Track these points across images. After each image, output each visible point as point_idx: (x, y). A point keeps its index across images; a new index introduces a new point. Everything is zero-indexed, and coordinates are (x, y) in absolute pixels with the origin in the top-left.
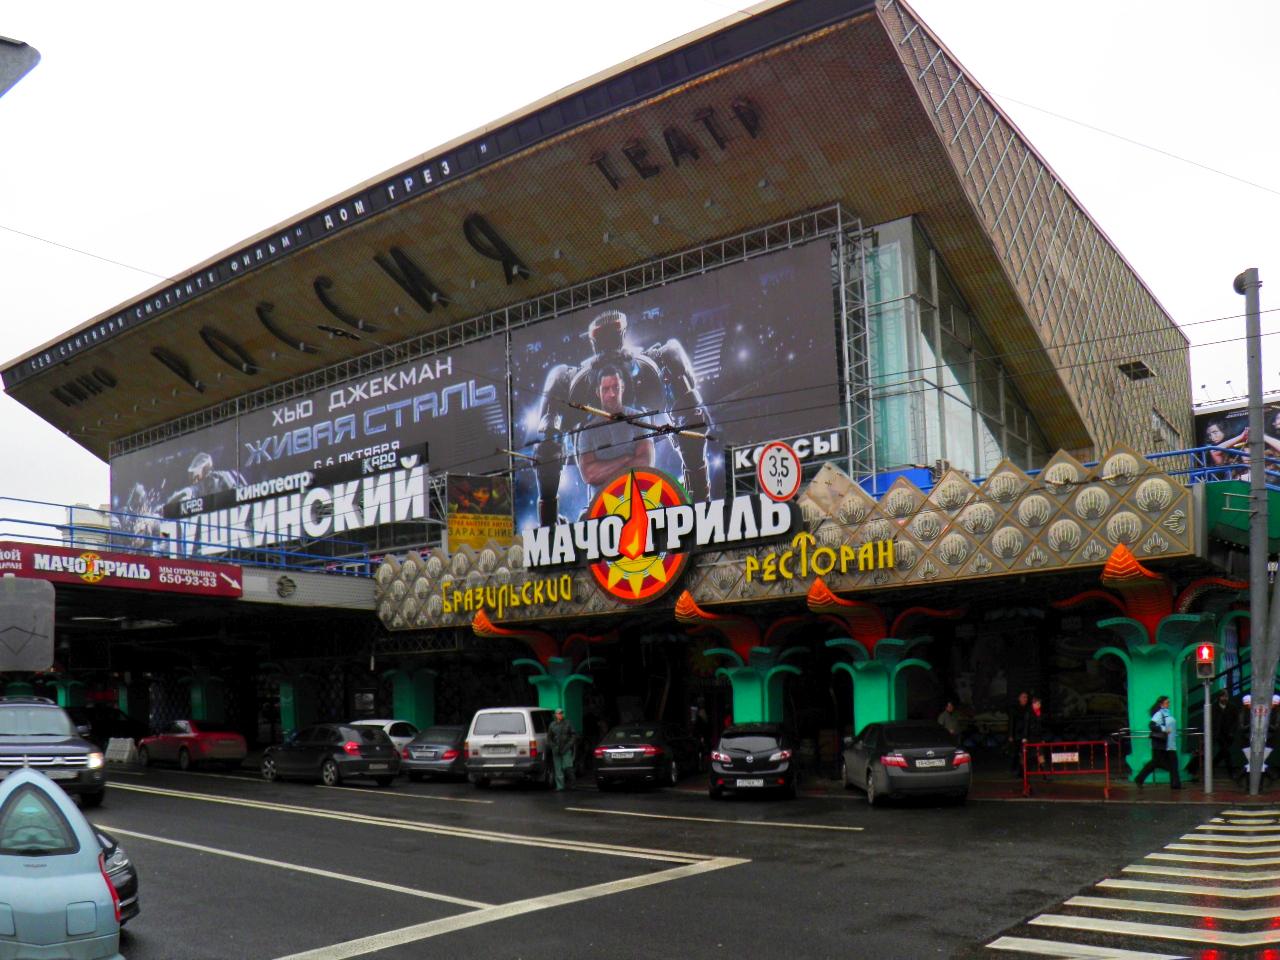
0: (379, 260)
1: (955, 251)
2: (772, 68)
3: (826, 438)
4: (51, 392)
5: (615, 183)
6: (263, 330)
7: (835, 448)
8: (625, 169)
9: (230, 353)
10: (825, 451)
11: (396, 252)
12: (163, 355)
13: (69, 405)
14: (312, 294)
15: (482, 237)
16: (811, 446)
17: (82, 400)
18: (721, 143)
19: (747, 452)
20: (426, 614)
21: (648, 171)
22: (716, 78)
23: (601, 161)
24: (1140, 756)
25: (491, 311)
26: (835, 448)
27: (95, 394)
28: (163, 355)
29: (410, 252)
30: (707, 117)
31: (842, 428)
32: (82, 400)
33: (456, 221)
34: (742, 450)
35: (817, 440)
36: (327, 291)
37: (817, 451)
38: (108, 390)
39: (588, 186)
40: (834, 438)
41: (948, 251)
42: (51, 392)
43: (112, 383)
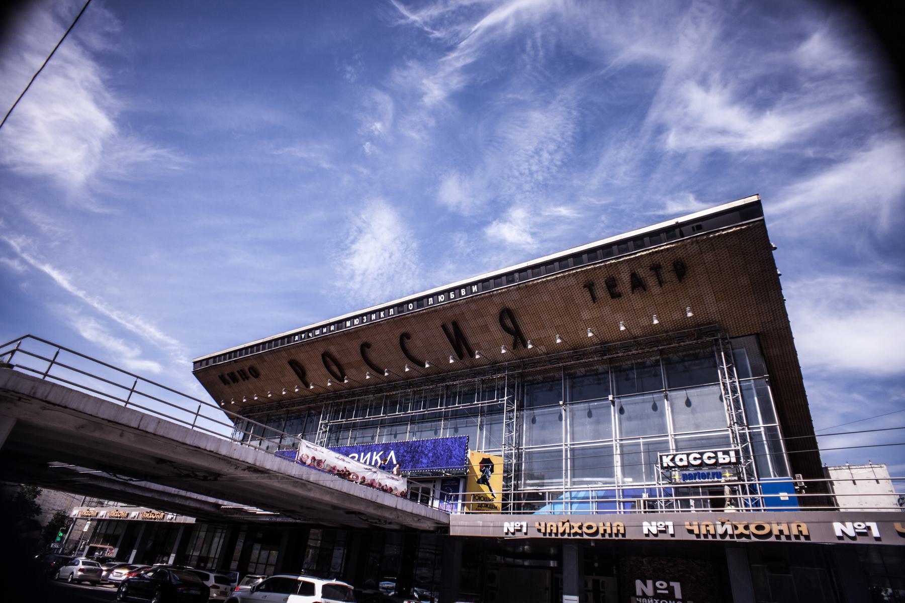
0: (444, 327)
1: (774, 356)
2: (699, 246)
3: (726, 453)
4: (219, 376)
5: (594, 299)
6: (359, 358)
7: (734, 460)
8: (601, 292)
9: (335, 368)
10: (727, 460)
11: (455, 324)
12: (294, 364)
13: (225, 385)
14: (396, 341)
15: (509, 323)
16: (716, 457)
17: (234, 383)
18: (661, 283)
19: (670, 457)
20: (110, 571)
21: (615, 295)
22: (667, 249)
23: (590, 286)
24: (222, 598)
25: (497, 364)
26: (734, 460)
27: (244, 380)
28: (294, 364)
29: (463, 326)
30: (656, 269)
31: (516, 492)
32: (234, 383)
33: (495, 311)
34: (667, 456)
35: (720, 455)
36: (406, 341)
37: (721, 461)
38: (252, 379)
39: (577, 300)
40: (732, 454)
41: (771, 356)
42: (219, 376)
43: (256, 375)
